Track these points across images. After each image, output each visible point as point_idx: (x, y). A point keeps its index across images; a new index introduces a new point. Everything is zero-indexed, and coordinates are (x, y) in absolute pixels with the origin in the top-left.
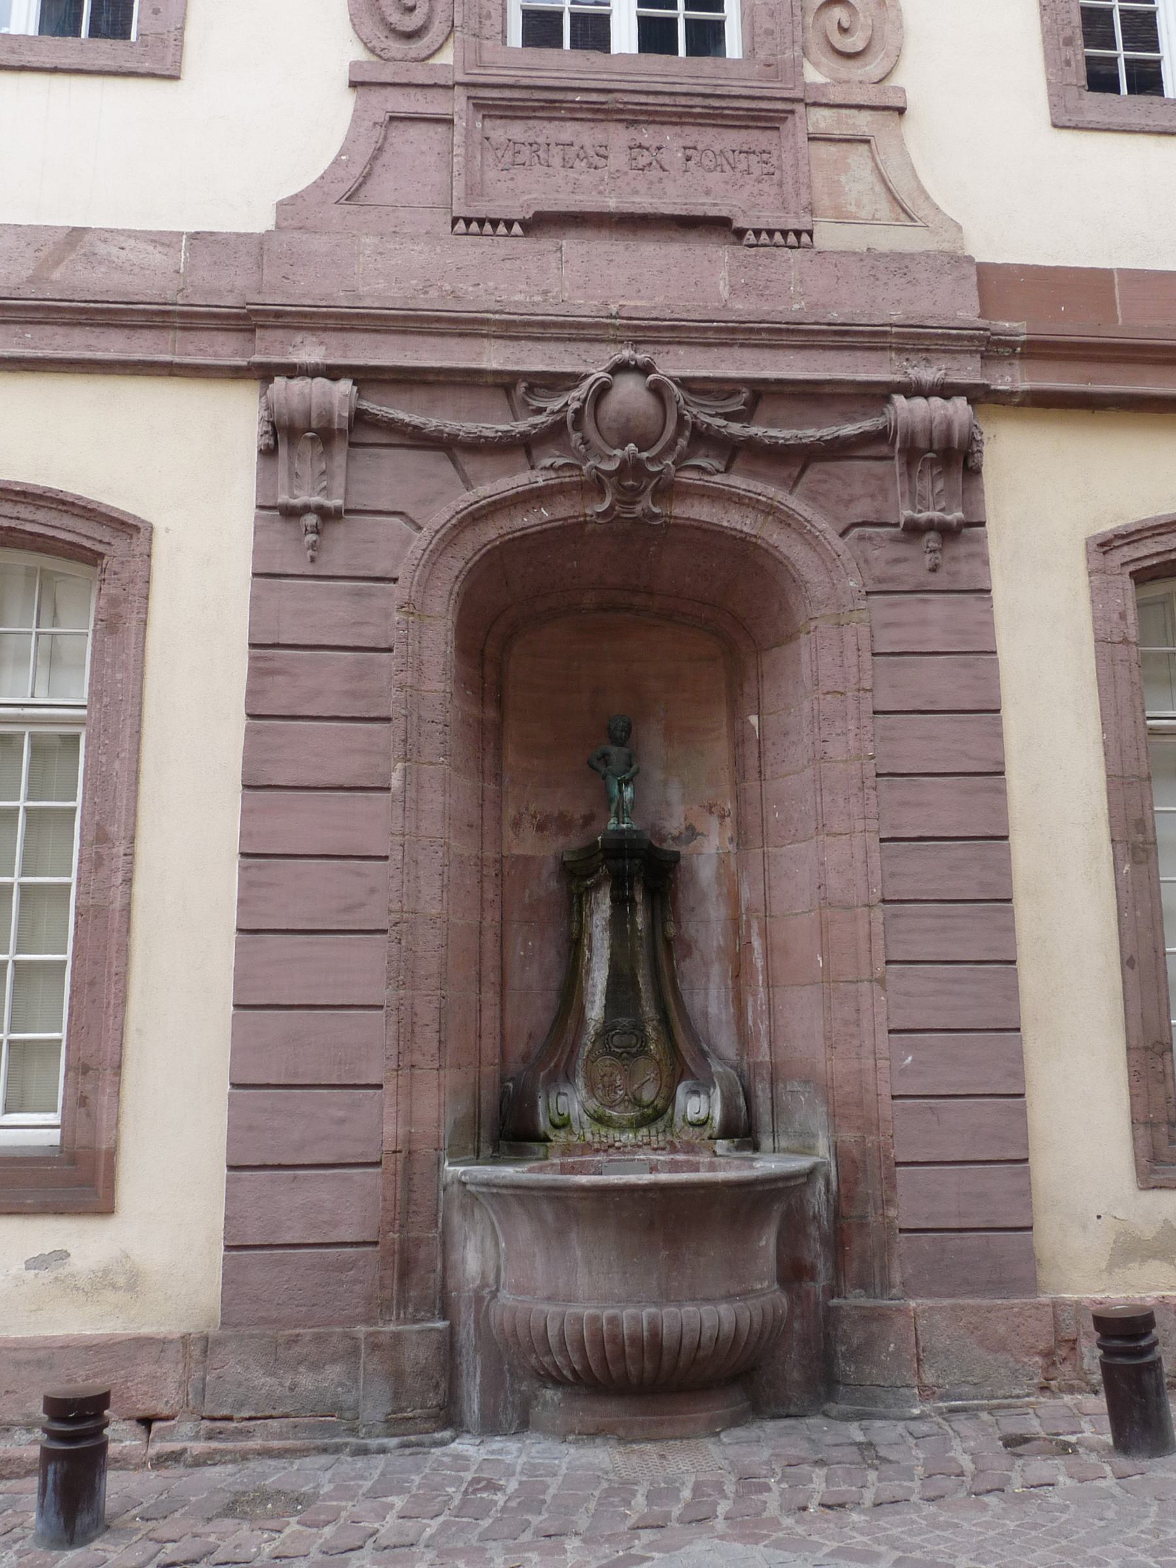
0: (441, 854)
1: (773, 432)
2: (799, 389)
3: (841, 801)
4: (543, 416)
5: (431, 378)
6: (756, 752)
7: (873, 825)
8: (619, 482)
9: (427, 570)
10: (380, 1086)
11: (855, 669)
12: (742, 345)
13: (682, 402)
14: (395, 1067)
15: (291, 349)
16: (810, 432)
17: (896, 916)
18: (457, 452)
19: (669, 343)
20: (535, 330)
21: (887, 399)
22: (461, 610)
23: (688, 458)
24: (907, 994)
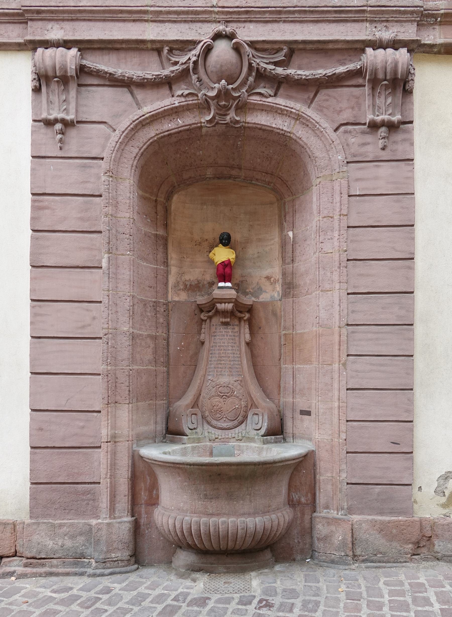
0: (128, 300)
1: (299, 72)
2: (315, 46)
3: (329, 274)
4: (180, 66)
5: (118, 46)
6: (291, 249)
7: (345, 286)
8: (217, 102)
9: (119, 154)
10: (99, 412)
11: (338, 204)
12: (285, 22)
13: (251, 56)
14: (106, 403)
15: (46, 32)
16: (320, 71)
17: (353, 332)
18: (133, 88)
19: (245, 22)
20: (172, 16)
21: (363, 51)
22: (141, 176)
23: (253, 89)
24: (357, 371)
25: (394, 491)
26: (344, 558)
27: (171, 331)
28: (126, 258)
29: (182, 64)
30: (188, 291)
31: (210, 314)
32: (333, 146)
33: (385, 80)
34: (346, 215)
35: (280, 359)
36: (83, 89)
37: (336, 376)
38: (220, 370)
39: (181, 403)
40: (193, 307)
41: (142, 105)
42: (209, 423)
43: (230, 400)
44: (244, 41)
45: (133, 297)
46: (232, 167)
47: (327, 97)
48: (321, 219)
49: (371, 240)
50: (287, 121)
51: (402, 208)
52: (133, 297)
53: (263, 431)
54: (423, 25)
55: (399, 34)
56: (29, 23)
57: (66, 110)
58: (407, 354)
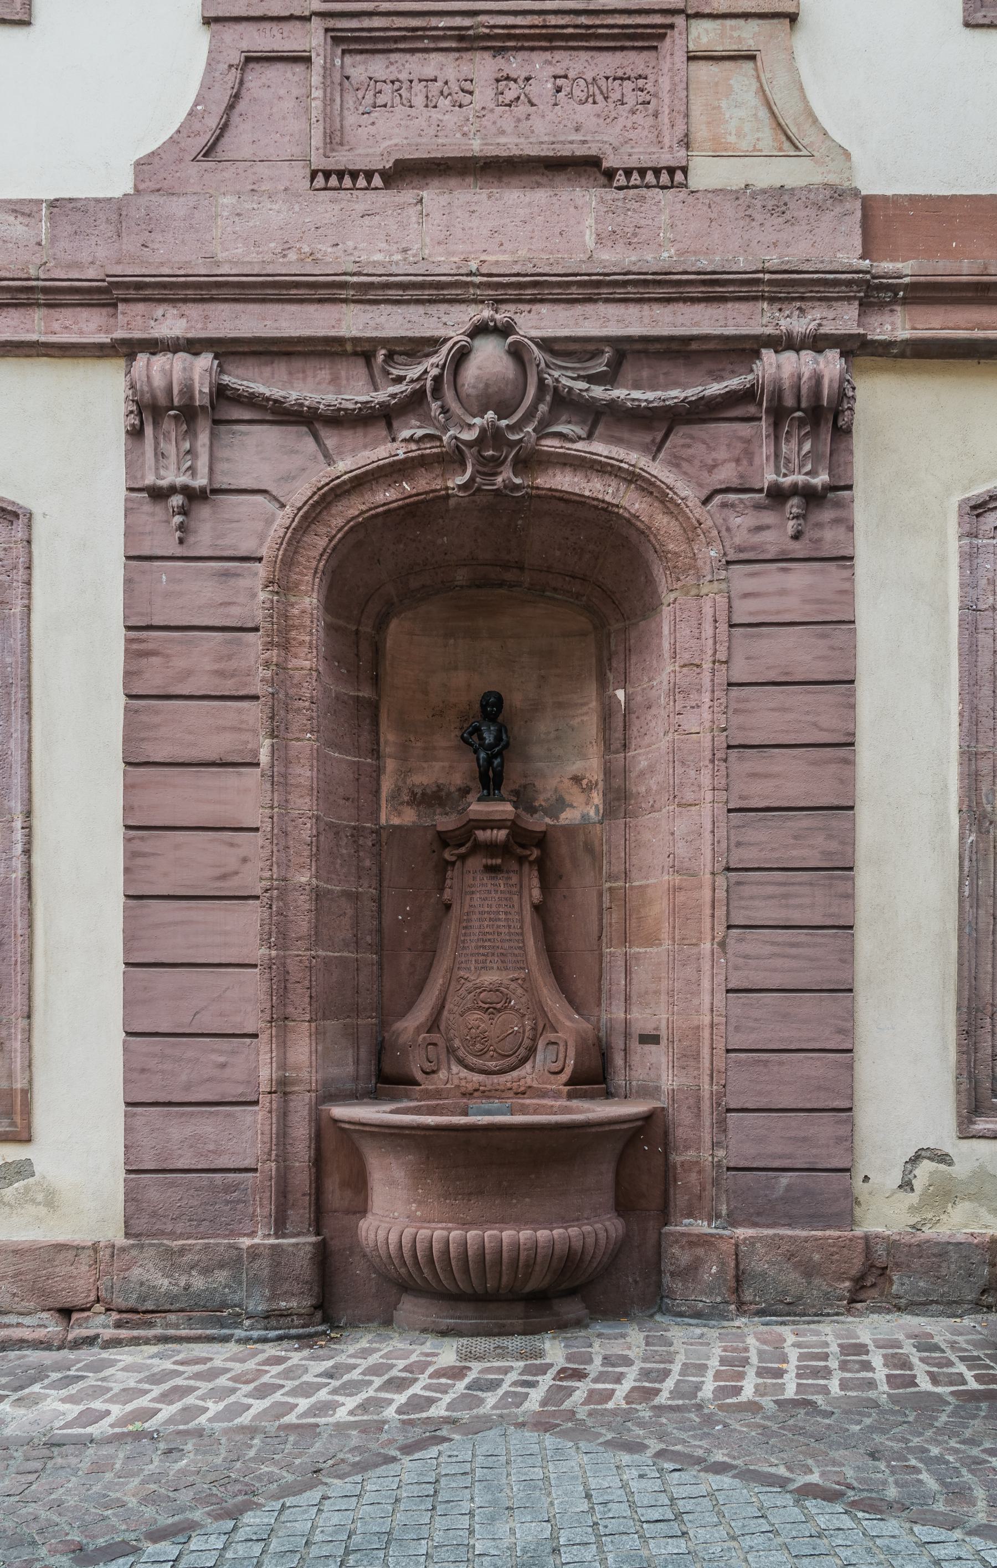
0: (309, 825)
1: (636, 394)
3: (692, 773)
6: (621, 725)
7: (723, 796)
8: (479, 452)
10: (255, 1036)
11: (711, 641)
12: (607, 301)
13: (543, 365)
15: (152, 323)
16: (674, 393)
17: (738, 883)
18: (318, 426)
21: (757, 355)
22: (330, 588)
24: (746, 957)
25: (825, 1186)
26: (721, 1306)
27: (385, 884)
28: (305, 744)
29: (412, 381)
30: (418, 805)
31: (463, 850)
32: (699, 531)
33: (799, 409)
34: (726, 662)
35: (600, 937)
36: (223, 428)
37: (706, 966)
38: (481, 958)
39: (406, 1024)
40: (429, 837)
41: (335, 457)
42: (462, 1062)
43: (503, 1017)
44: (531, 339)
45: (318, 818)
46: (506, 566)
47: (688, 441)
48: (678, 669)
49: (772, 710)
50: (613, 484)
51: (832, 648)
52: (318, 818)
53: (565, 1077)
54: (871, 305)
55: (824, 322)
56: (121, 307)
57: (192, 470)
58: (842, 923)
